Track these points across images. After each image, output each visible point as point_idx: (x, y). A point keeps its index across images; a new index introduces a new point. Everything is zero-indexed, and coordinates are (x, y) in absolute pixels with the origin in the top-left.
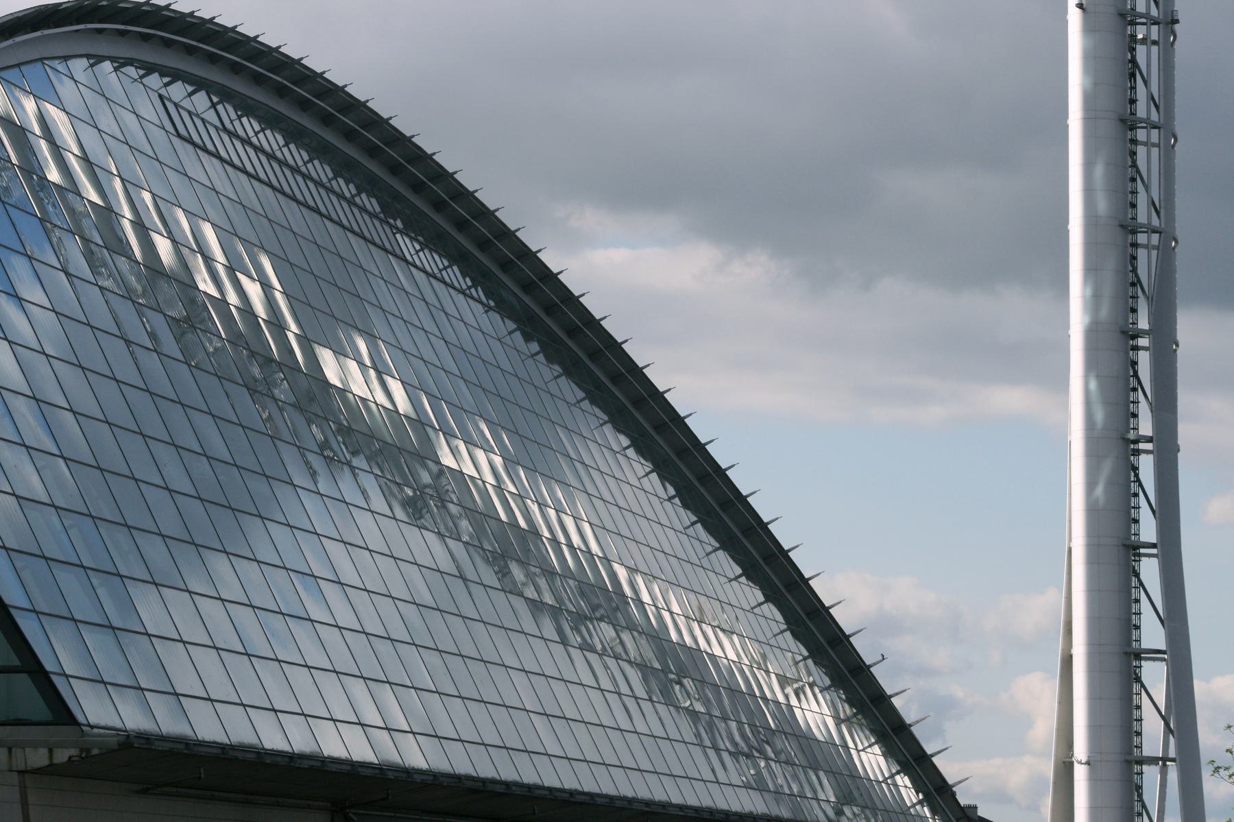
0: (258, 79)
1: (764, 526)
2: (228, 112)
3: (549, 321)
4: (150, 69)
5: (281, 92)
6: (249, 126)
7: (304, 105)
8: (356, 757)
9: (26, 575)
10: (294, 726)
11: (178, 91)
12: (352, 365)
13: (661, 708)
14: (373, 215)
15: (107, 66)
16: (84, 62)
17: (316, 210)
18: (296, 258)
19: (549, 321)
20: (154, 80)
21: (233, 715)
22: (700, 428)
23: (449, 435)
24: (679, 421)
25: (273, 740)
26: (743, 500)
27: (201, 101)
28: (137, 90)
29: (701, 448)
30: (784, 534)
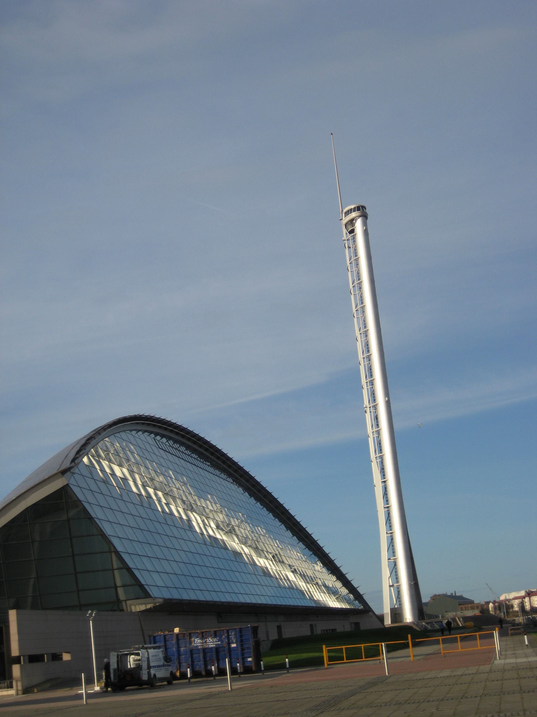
0: (177, 434)
1: (310, 535)
2: (171, 442)
3: (229, 470)
4: (151, 433)
5: (183, 436)
6: (176, 446)
7: (189, 439)
8: (215, 600)
9: (154, 563)
10: (191, 593)
11: (158, 438)
12: (208, 502)
13: (322, 594)
14: (209, 466)
15: (140, 433)
16: (135, 432)
17: (195, 465)
18: (191, 476)
19: (253, 489)
20: (153, 435)
21: (227, 595)
22: (264, 484)
23: (233, 518)
24: (293, 517)
25: (185, 597)
26: (304, 529)
27: (164, 440)
28: (148, 438)
29: (293, 517)
30: (315, 537)
